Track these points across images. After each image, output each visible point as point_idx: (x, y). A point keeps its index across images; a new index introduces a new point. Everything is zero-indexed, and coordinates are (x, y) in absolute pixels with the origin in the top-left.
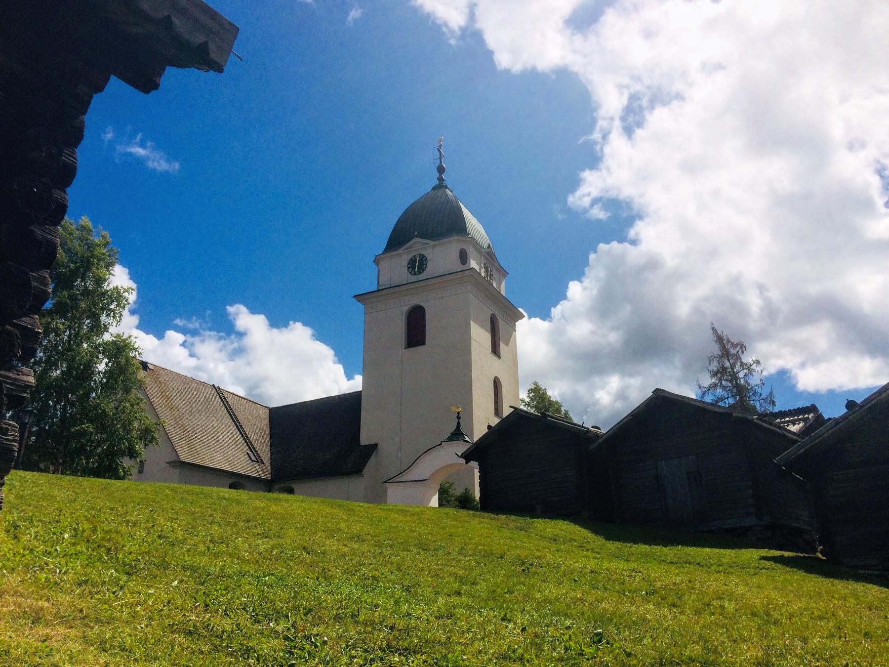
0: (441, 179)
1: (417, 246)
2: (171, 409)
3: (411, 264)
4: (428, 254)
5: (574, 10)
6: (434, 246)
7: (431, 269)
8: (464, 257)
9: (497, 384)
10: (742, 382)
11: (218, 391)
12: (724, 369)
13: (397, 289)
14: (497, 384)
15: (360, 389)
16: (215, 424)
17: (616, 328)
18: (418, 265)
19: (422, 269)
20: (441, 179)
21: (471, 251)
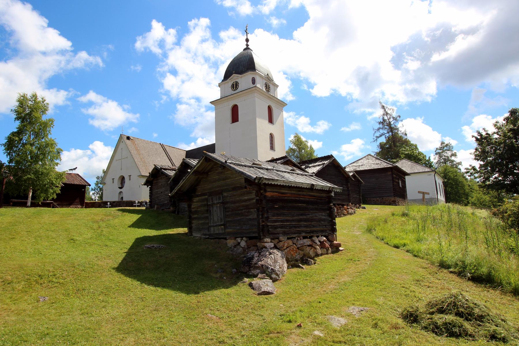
0: (247, 45)
1: (235, 77)
2: (139, 155)
3: (233, 86)
4: (239, 81)
5: (12, 33)
6: (241, 77)
7: (240, 88)
8: (254, 81)
9: (272, 136)
10: (393, 126)
11: (162, 146)
12: (384, 120)
13: (226, 98)
14: (272, 136)
15: (214, 142)
16: (159, 159)
17: (407, 93)
18: (235, 86)
19: (237, 88)
20: (247, 45)
21: (258, 79)
